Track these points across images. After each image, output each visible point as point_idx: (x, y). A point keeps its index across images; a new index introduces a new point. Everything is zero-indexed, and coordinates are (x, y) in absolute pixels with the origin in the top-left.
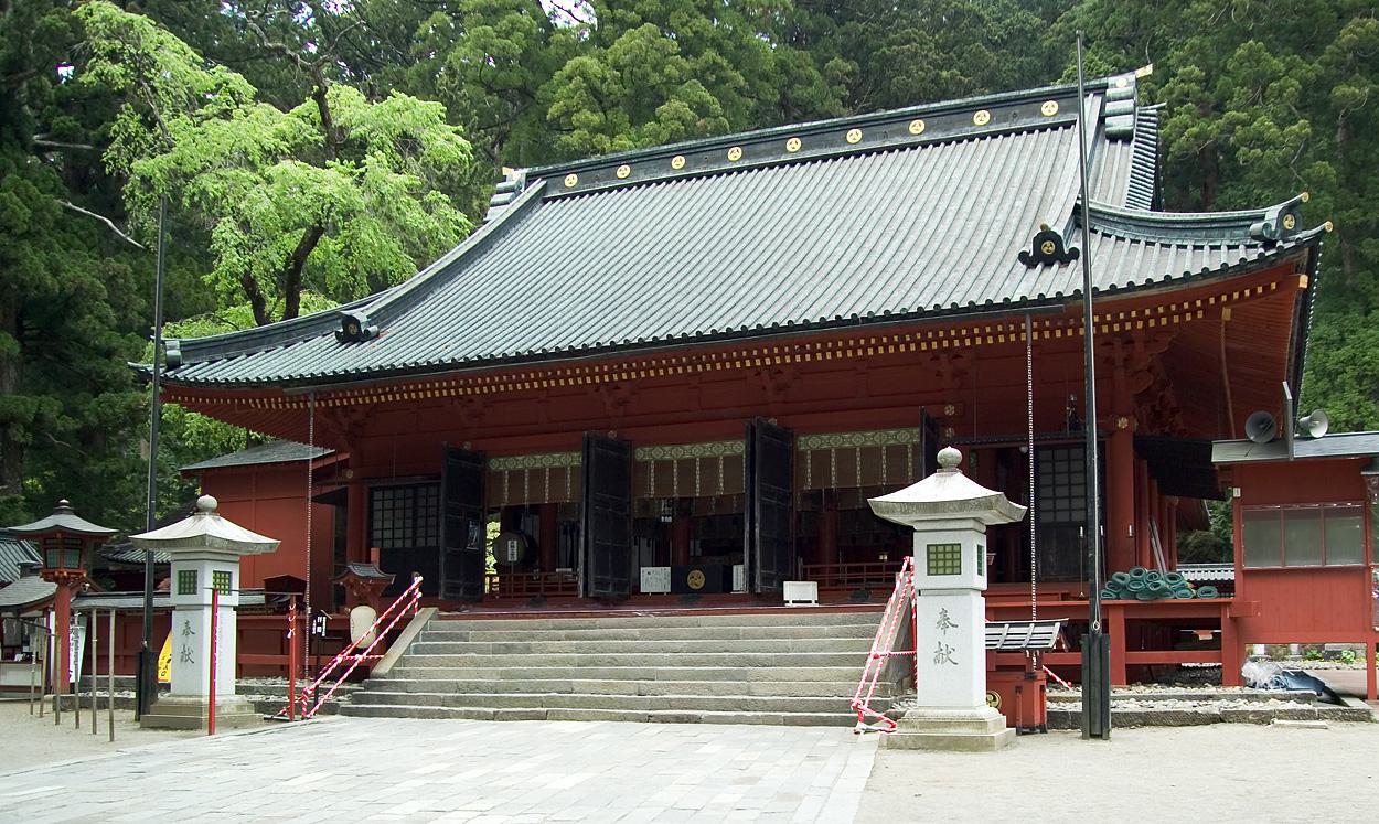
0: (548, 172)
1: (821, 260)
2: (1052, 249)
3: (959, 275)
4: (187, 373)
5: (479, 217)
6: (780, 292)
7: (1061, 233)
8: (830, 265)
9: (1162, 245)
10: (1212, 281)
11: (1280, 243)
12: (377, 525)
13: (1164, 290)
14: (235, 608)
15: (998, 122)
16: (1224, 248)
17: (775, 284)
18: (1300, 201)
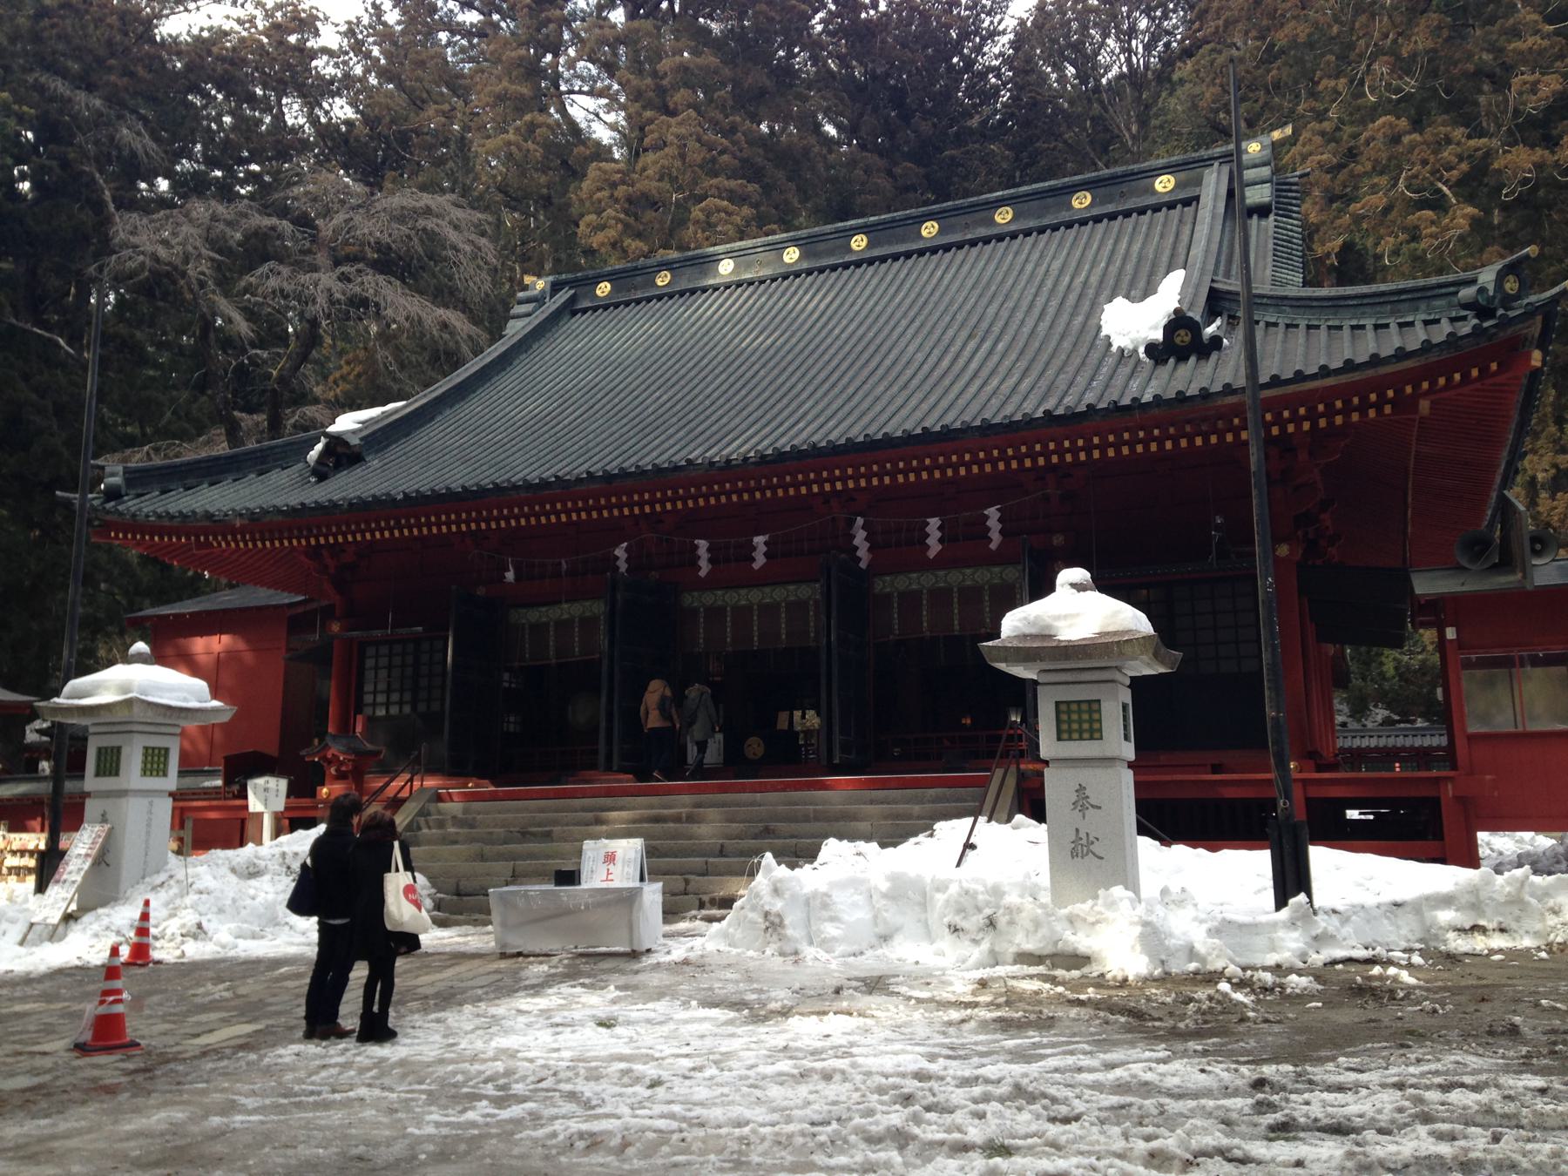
0: (576, 280)
1: (898, 368)
2: (1187, 339)
3: (1070, 376)
4: (130, 505)
5: (496, 334)
6: (852, 404)
7: (1198, 318)
8: (909, 372)
9: (1330, 327)
10: (1409, 364)
11: (1500, 312)
12: (369, 687)
13: (1344, 379)
14: (171, 794)
15: (1102, 203)
16: (1419, 326)
17: (844, 396)
18: (1527, 256)
